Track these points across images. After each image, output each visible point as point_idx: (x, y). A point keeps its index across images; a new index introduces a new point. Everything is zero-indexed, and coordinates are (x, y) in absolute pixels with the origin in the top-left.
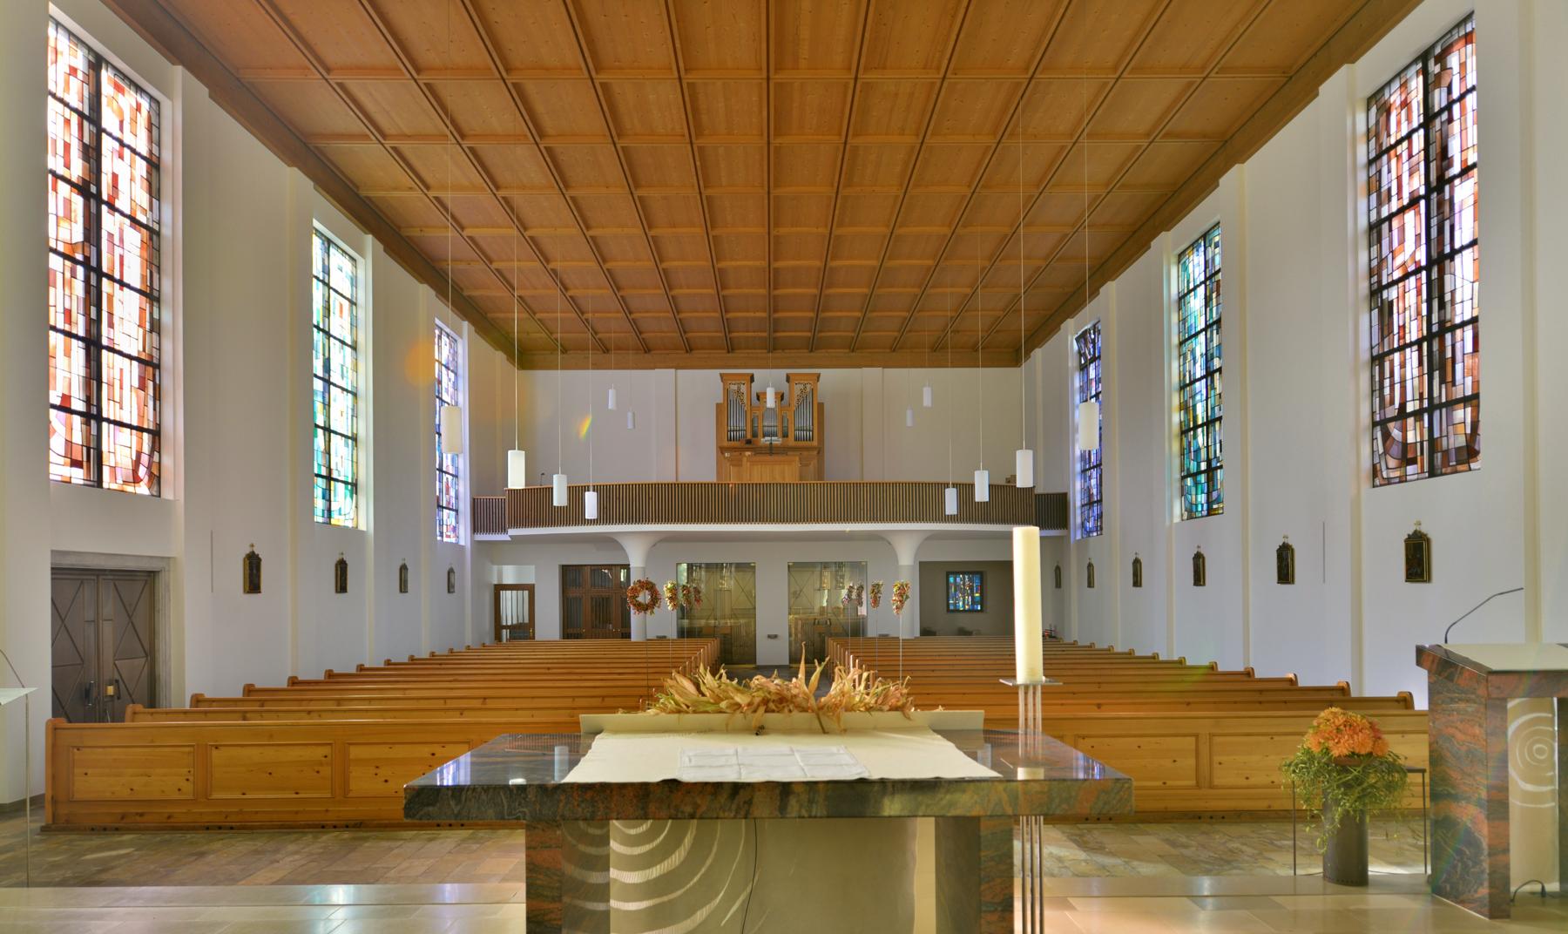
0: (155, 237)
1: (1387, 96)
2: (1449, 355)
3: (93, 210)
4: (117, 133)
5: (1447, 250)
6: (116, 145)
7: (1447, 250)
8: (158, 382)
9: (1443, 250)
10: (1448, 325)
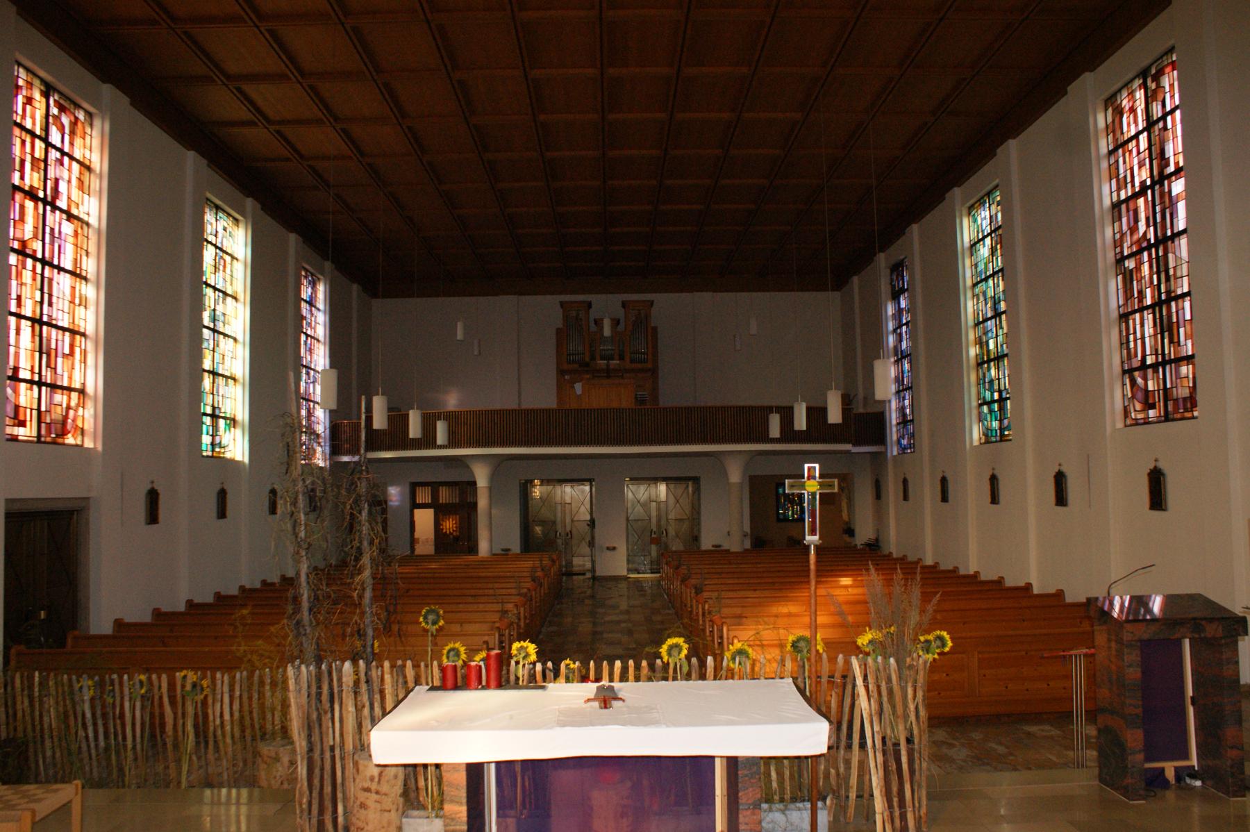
0: (85, 227)
1: (1119, 102)
2: (1174, 320)
3: (41, 211)
4: (59, 145)
5: (1169, 233)
6: (58, 155)
7: (1169, 233)
8: (83, 347)
9: (1166, 233)
10: (1173, 295)
